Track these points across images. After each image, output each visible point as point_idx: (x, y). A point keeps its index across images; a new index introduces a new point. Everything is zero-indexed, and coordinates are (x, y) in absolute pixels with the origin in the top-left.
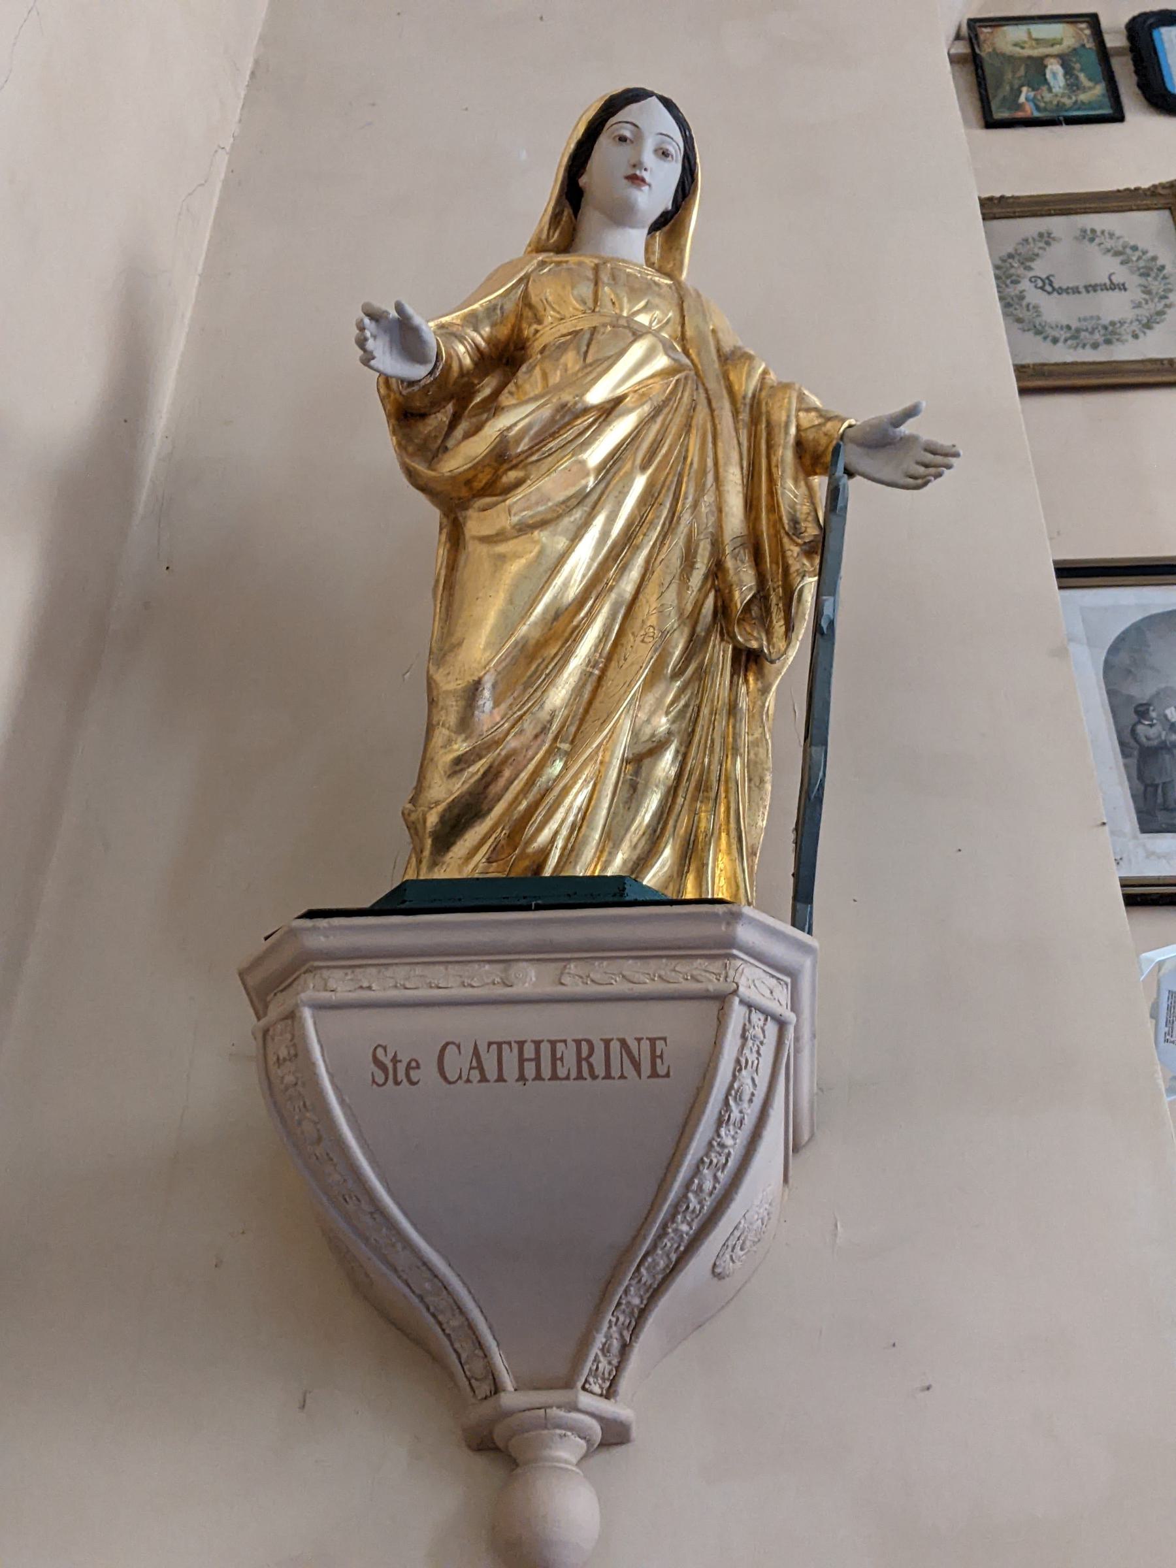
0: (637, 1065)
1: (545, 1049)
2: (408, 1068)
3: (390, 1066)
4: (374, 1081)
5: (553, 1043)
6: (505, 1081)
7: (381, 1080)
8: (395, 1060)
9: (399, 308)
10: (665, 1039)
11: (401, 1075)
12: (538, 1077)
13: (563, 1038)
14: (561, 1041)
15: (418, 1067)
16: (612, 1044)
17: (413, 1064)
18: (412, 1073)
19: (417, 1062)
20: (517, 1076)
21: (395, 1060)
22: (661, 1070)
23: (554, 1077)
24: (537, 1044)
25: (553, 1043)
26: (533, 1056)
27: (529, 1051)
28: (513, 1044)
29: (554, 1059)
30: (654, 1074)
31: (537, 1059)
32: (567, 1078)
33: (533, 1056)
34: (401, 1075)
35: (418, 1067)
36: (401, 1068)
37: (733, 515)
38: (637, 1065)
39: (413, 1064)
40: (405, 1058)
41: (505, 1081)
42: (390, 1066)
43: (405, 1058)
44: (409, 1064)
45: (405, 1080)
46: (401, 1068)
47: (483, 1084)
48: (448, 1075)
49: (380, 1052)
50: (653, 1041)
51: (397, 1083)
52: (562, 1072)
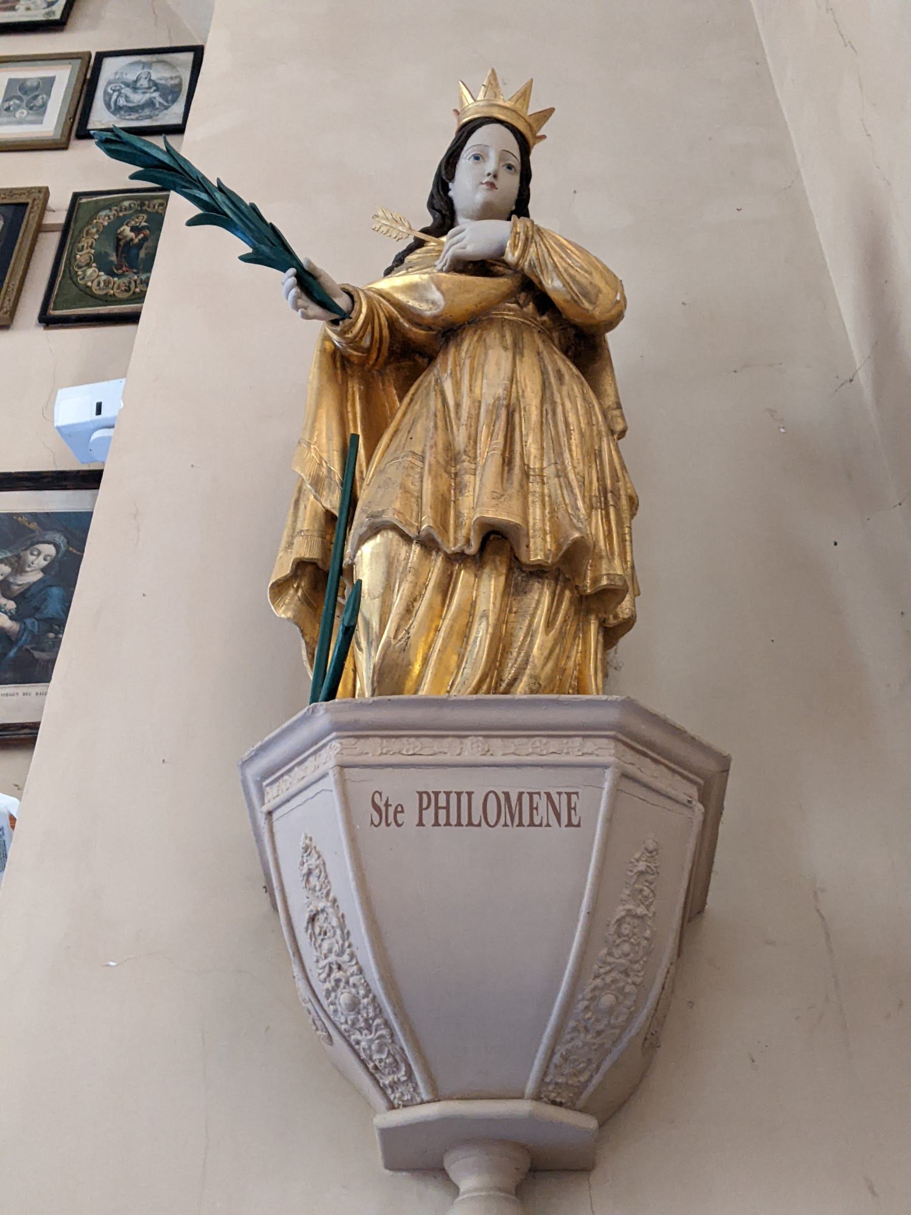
0: (558, 816)
1: (526, 799)
2: (396, 812)
3: (383, 809)
4: (372, 823)
5: (531, 795)
6: (423, 825)
7: (376, 822)
8: (387, 805)
9: (544, 137)
10: (577, 793)
11: (391, 819)
12: (448, 824)
13: (537, 791)
14: (574, 793)
15: (402, 812)
16: (440, 795)
17: (399, 809)
18: (398, 815)
19: (402, 807)
20: (433, 822)
21: (387, 805)
22: (575, 821)
23: (532, 824)
24: (448, 794)
25: (531, 795)
26: (444, 805)
27: (442, 802)
28: (542, 794)
29: (532, 808)
30: (570, 824)
31: (447, 808)
32: (541, 825)
33: (444, 805)
34: (391, 819)
35: (402, 812)
36: (391, 810)
37: (608, 395)
38: (558, 816)
39: (399, 809)
40: (394, 803)
41: (423, 825)
42: (383, 809)
43: (394, 803)
44: (396, 808)
45: (393, 823)
46: (391, 810)
47: (421, 828)
48: (489, 820)
49: (377, 796)
50: (569, 795)
51: (388, 825)
52: (537, 821)
